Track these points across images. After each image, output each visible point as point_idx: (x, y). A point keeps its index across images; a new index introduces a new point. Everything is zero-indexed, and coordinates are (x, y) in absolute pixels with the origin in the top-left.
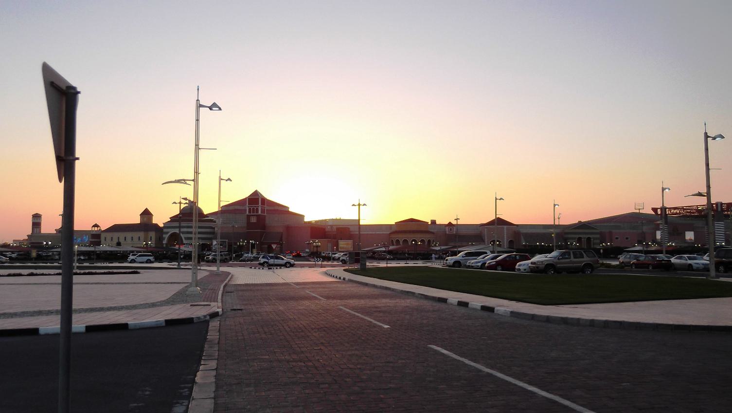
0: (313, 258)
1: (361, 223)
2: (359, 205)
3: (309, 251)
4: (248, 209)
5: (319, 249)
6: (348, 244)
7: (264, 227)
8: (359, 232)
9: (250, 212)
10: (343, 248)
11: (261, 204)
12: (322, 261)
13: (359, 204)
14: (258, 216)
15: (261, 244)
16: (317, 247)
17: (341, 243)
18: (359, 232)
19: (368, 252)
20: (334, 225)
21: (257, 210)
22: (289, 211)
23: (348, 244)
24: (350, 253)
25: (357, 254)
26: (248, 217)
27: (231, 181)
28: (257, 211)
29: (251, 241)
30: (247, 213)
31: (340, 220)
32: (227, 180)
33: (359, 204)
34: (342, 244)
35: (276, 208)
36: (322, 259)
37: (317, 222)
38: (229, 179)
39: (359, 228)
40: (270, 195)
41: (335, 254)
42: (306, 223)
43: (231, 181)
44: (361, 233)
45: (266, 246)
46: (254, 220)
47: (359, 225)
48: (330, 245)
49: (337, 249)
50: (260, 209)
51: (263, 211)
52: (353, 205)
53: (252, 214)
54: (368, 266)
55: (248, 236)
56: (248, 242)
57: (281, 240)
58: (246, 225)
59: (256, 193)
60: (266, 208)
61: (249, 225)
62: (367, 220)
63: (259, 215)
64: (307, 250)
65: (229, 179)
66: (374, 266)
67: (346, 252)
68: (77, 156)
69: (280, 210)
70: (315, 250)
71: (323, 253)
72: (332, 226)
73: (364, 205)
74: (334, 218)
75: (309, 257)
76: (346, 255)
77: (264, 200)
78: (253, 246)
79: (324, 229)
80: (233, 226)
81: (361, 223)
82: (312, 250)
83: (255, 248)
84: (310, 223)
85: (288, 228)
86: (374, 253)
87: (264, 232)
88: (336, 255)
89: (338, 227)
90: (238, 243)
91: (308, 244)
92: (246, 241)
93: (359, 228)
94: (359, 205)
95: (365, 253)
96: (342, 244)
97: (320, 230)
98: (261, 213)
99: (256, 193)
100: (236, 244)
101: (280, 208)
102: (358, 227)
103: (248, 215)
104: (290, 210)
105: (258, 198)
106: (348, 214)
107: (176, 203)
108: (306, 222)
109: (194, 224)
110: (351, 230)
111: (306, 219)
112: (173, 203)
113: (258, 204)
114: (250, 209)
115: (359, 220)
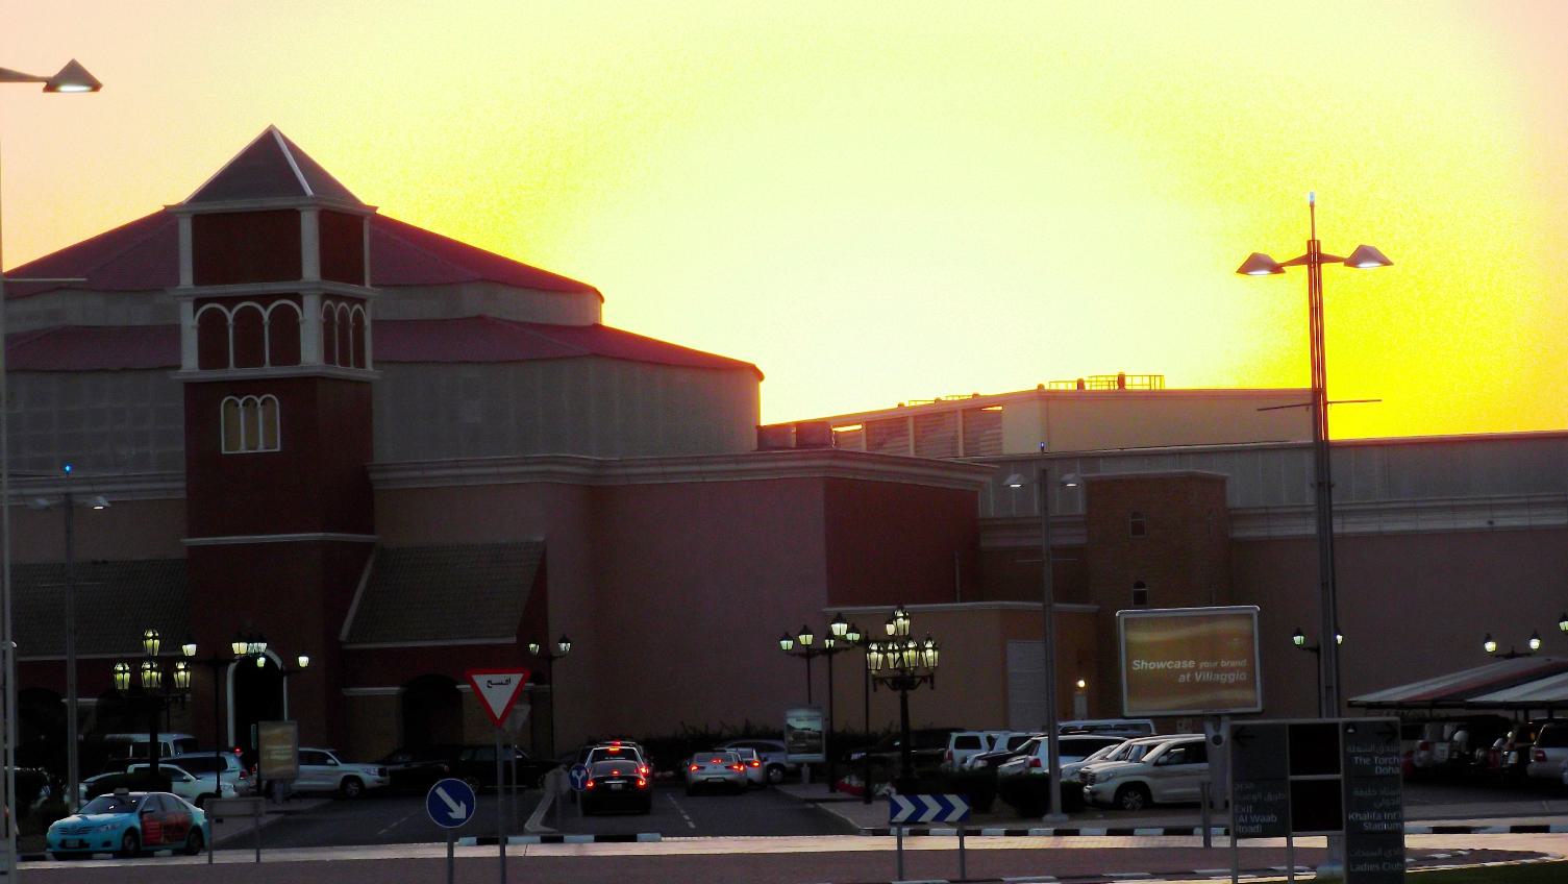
0: (867, 796)
1: (1343, 426)
2: (1314, 259)
3: (816, 726)
4: (189, 322)
5: (925, 711)
6: (1209, 648)
7: (357, 499)
8: (1325, 514)
9: (211, 354)
10: (1164, 684)
11: (326, 273)
12: (965, 829)
13: (1313, 245)
14: (298, 393)
15: (341, 666)
16: (904, 680)
17: (1141, 637)
18: (1325, 514)
19: (1413, 720)
20: (1069, 460)
21: (287, 325)
22: (599, 330)
23: (1209, 648)
24: (1239, 735)
25: (1314, 746)
26: (202, 401)
27: (95, 86)
28: (288, 349)
29: (240, 648)
30: (190, 361)
31: (1120, 397)
32: (52, 86)
33: (1313, 245)
34: (1152, 642)
35: (473, 301)
36: (960, 807)
37: (885, 426)
38: (74, 74)
39: (1324, 486)
40: (402, 167)
41: (1085, 749)
42: (772, 438)
43: (95, 86)
44: (1337, 528)
45: (394, 690)
46: (253, 430)
47: (1323, 449)
48: (1026, 660)
49: (1106, 700)
50: (310, 318)
51: (342, 339)
52: (1255, 264)
53: (233, 372)
54: (1425, 856)
55: (203, 600)
56: (213, 661)
57: (534, 623)
58: (178, 487)
59: (268, 161)
60: (375, 301)
61: (217, 484)
62: (1385, 399)
63: (310, 381)
64: (802, 721)
65: (74, 74)
66: (1485, 854)
67: (1196, 724)
68: (1038, 450)
69: (511, 324)
70: (885, 713)
71: (964, 743)
72: (1043, 468)
73: (1363, 255)
74: (1061, 379)
75: (821, 791)
76: (1194, 753)
77: (350, 228)
78: (260, 693)
79: (962, 503)
80: (68, 504)
81: (1343, 426)
82: (851, 719)
83: (275, 716)
84: (811, 437)
85: (600, 501)
86: (1485, 725)
87: (369, 546)
88: (1096, 764)
89: (1107, 471)
90: (123, 675)
91: (808, 653)
92: (190, 649)
93: (1324, 486)
94: (1314, 259)
95: (1387, 733)
96: (1152, 642)
97: (934, 511)
98: (329, 357)
99: (268, 161)
100: (97, 676)
101: (508, 305)
102: (1308, 461)
103: (192, 388)
104: (613, 316)
105: (292, 217)
106: (1187, 334)
107: (1277, 269)
108: (779, 430)
109: (367, 289)
110: (1236, 498)
111: (777, 407)
112: (1246, 269)
113: (296, 273)
114: (211, 327)
115: (1316, 400)
